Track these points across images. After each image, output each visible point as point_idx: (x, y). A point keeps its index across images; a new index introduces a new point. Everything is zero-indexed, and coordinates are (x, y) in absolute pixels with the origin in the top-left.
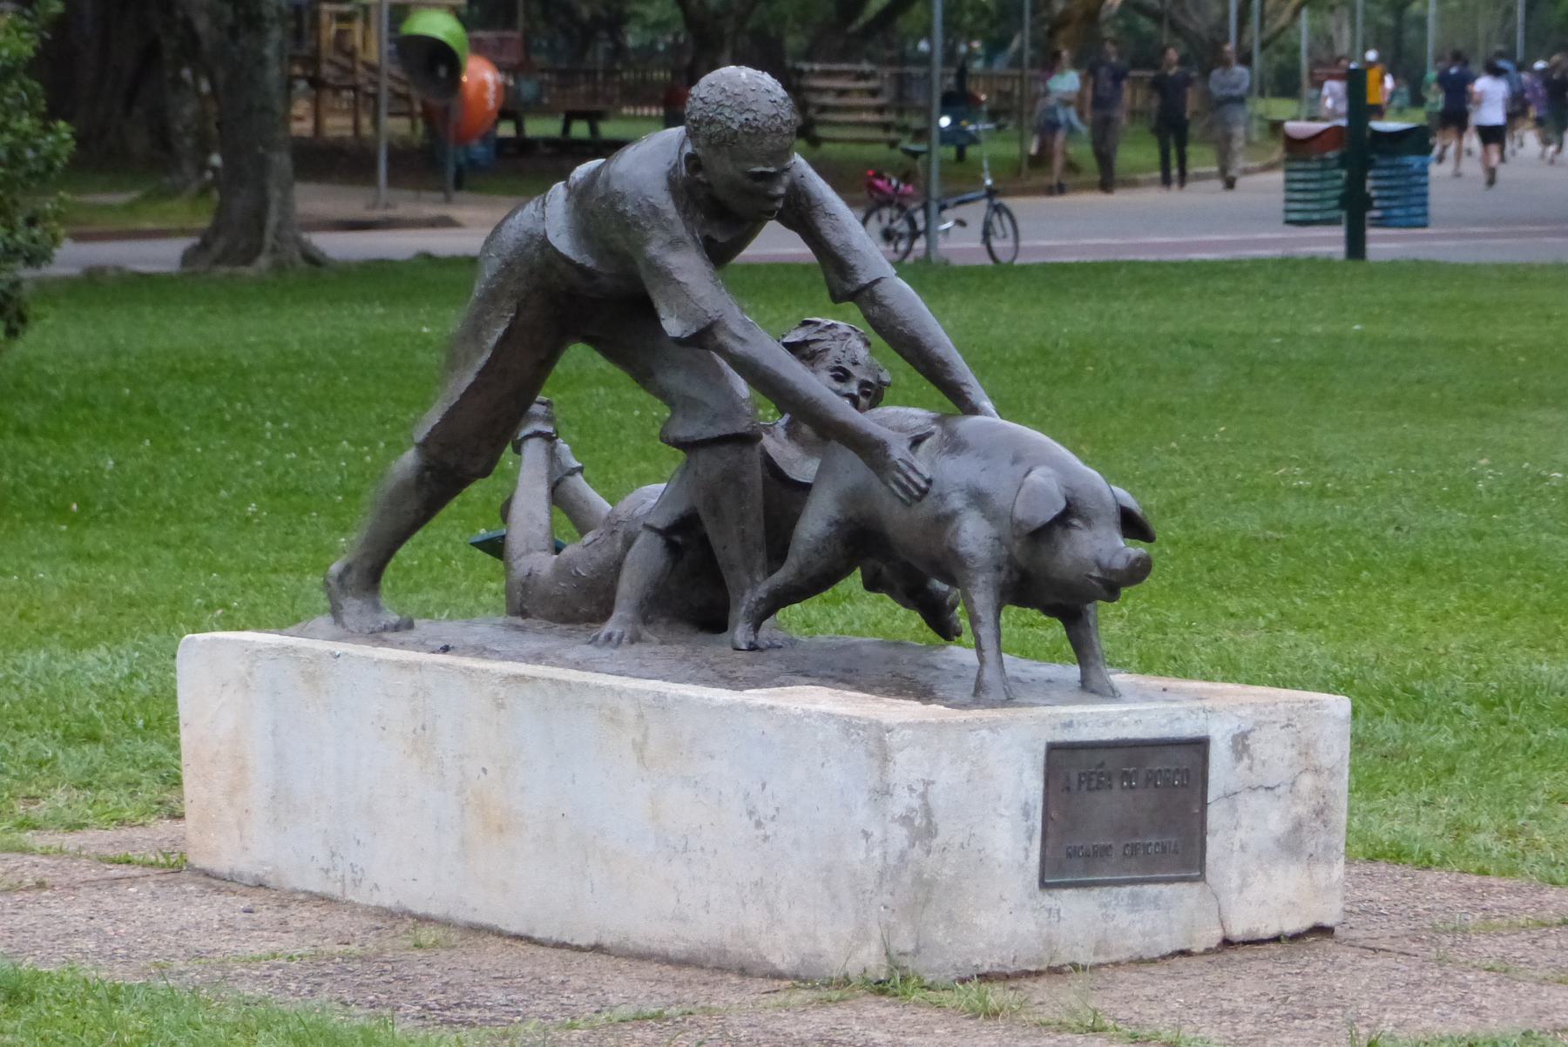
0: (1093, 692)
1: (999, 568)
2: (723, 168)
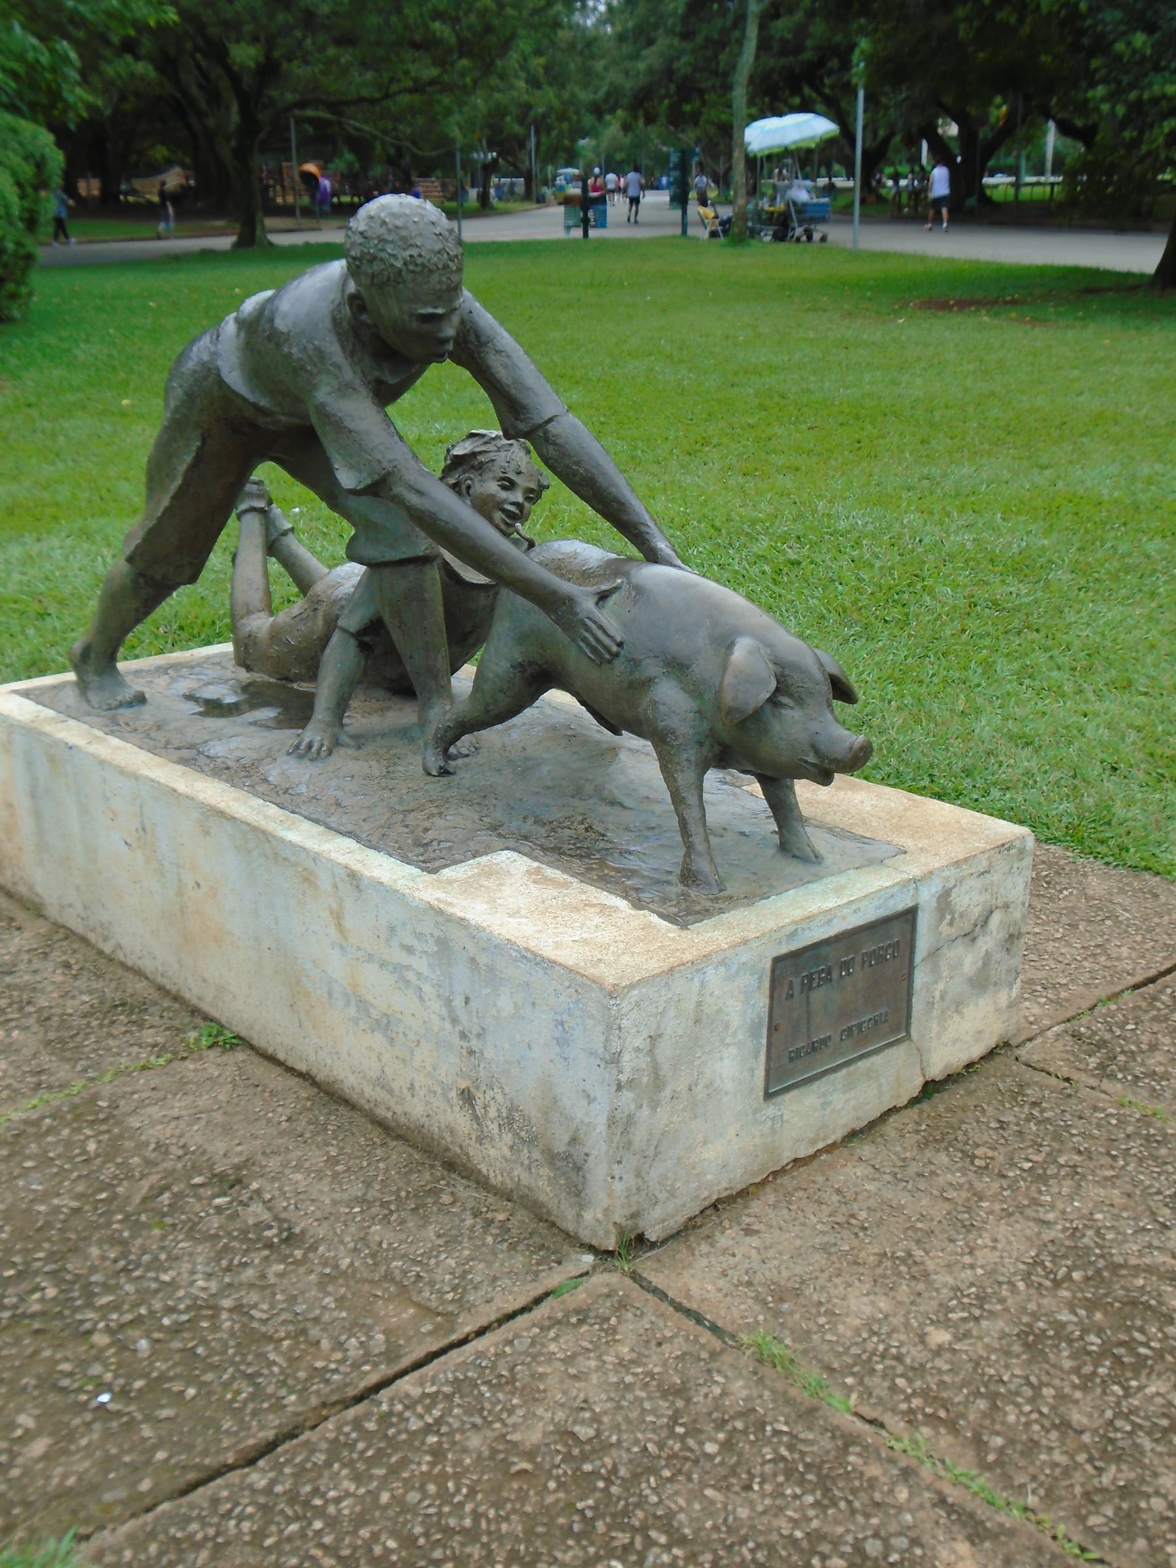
0: (794, 856)
1: (701, 744)
2: (393, 309)
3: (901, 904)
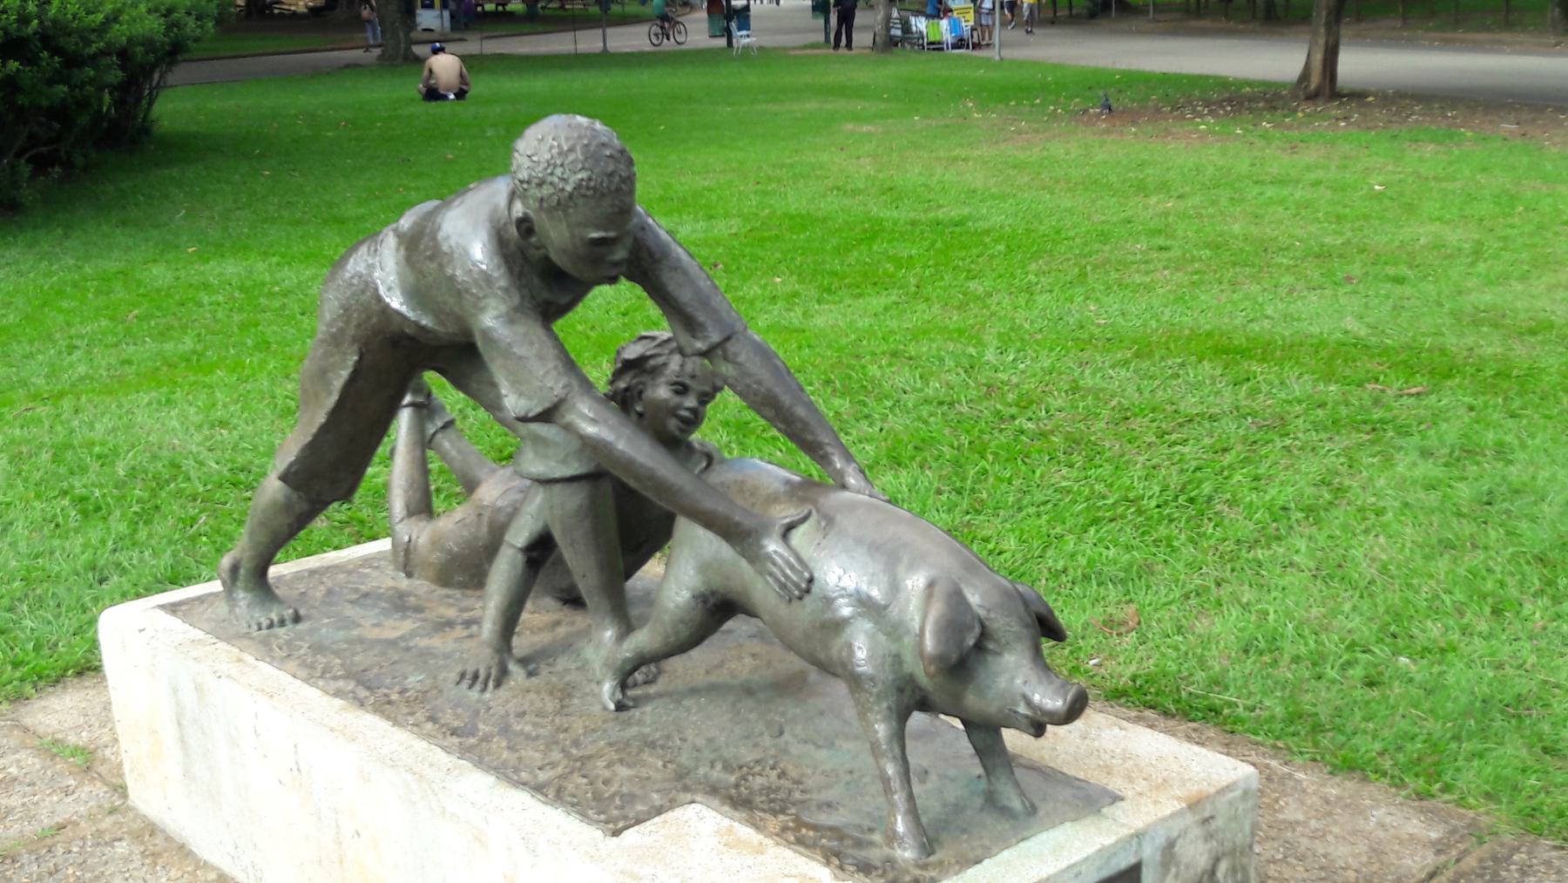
3: (1124, 862)
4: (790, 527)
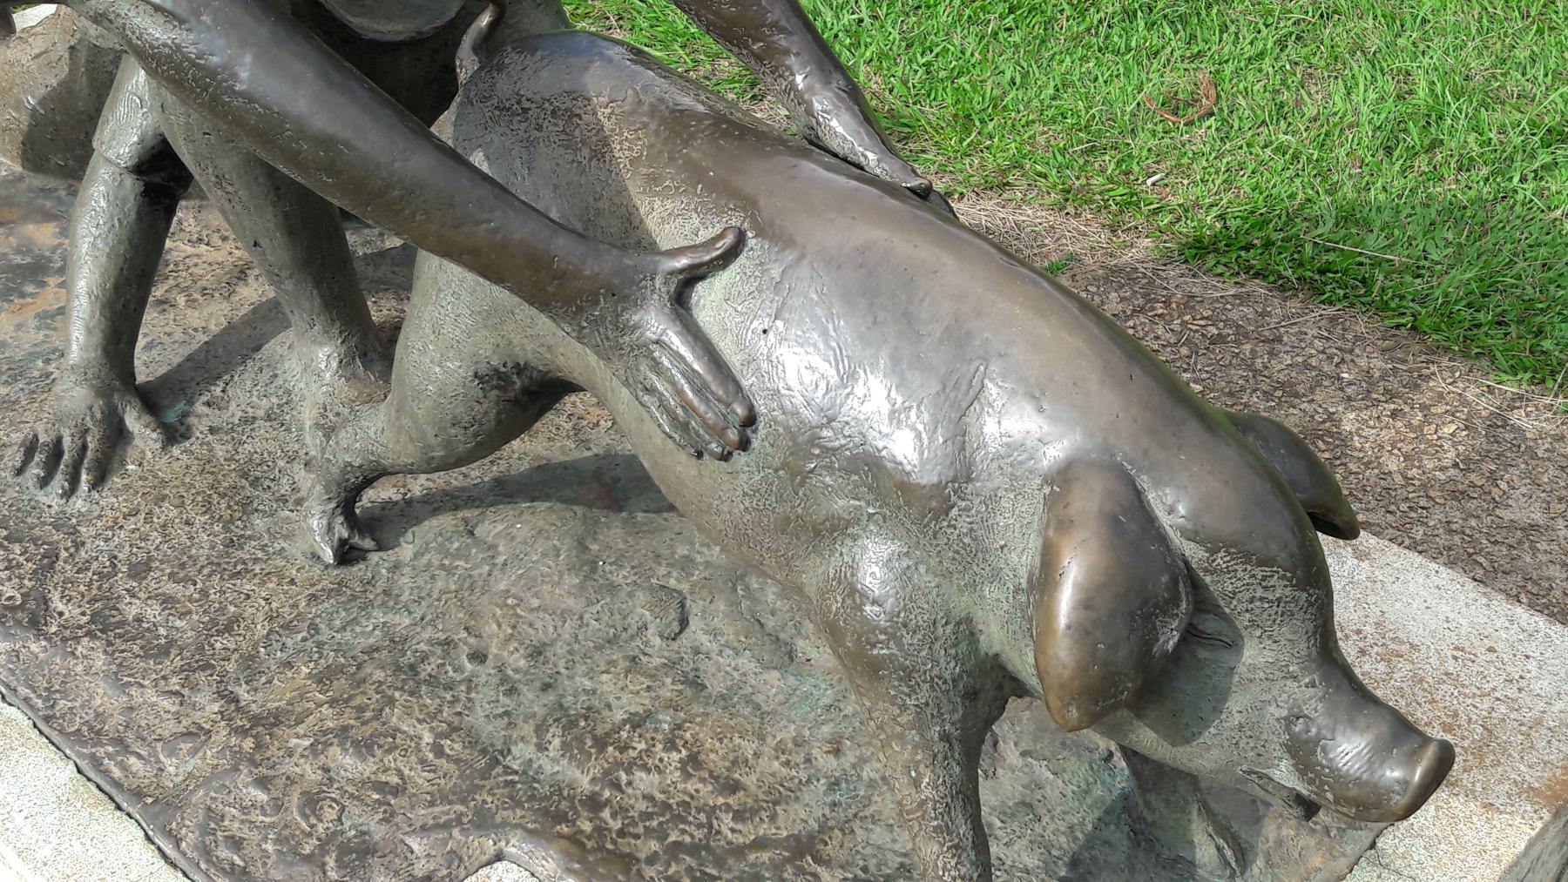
4: (692, 277)
